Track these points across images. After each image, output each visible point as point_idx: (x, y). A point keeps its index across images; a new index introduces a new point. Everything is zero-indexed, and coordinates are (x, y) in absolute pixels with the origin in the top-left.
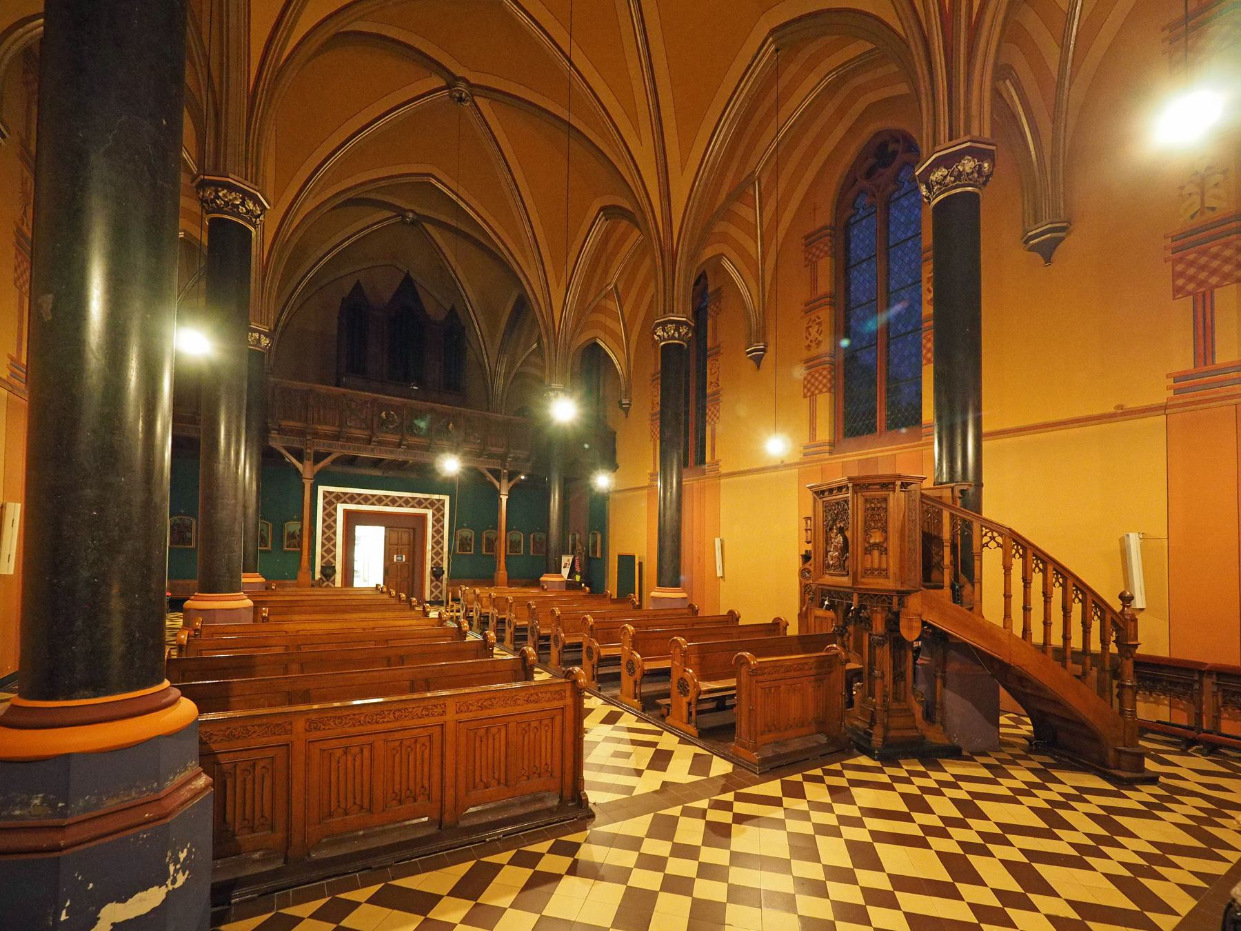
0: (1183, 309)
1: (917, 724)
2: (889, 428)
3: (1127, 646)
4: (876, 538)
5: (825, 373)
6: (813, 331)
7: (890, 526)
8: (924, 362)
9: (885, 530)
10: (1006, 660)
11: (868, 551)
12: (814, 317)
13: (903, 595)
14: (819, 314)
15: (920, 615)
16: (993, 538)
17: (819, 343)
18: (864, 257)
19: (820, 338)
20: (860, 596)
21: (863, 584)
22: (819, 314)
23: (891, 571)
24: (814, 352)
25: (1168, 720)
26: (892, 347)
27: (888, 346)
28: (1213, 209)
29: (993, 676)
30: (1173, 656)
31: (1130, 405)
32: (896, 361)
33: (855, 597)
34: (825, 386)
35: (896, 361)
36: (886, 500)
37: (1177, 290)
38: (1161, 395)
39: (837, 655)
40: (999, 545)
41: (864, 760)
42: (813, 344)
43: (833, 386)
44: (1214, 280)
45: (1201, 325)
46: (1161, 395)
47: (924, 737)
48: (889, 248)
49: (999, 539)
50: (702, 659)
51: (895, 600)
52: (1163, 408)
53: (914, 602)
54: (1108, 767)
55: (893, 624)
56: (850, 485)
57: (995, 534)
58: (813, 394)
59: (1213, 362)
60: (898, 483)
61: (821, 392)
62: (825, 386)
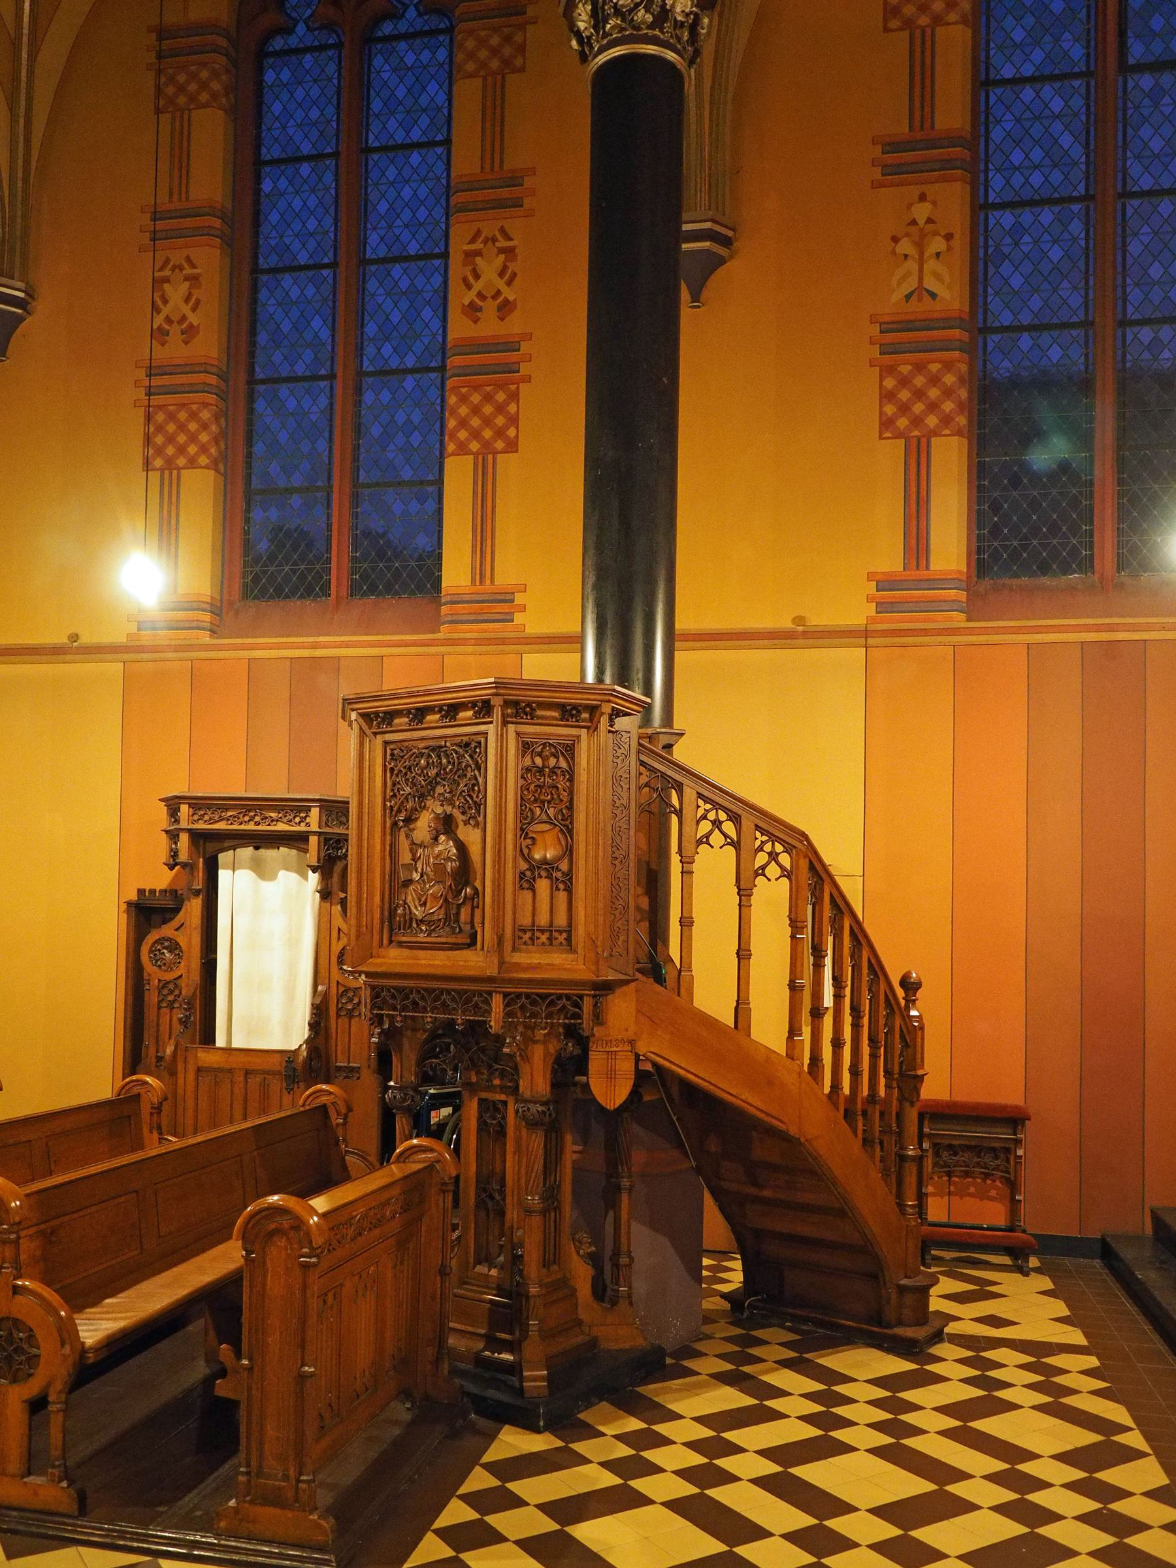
0: (890, 456)
1: (583, 1315)
2: (355, 590)
3: (908, 1078)
4: (546, 851)
5: (205, 415)
6: (176, 292)
7: (580, 817)
8: (451, 447)
9: (567, 828)
10: (793, 1131)
11: (526, 881)
12: (177, 257)
13: (604, 988)
14: (194, 253)
15: (632, 1042)
16: (773, 856)
17: (190, 332)
18: (306, 149)
19: (509, 294)
20: (510, 1000)
21: (517, 967)
22: (194, 253)
23: (580, 932)
24: (175, 351)
25: (945, 1220)
26: (368, 397)
27: (358, 391)
28: (933, 296)
29: (698, 1170)
30: (958, 1098)
31: (819, 619)
32: (376, 431)
33: (497, 1002)
34: (204, 449)
35: (376, 431)
36: (569, 750)
37: (886, 424)
38: (857, 611)
39: (430, 1168)
40: (786, 874)
41: (514, 1442)
42: (175, 330)
43: (223, 456)
44: (932, 421)
45: (914, 497)
46: (857, 611)
47: (593, 1343)
48: (259, 163)
49: (785, 859)
50: (48, 1237)
51: (587, 1004)
52: (862, 635)
53: (622, 1010)
54: (889, 1327)
55: (571, 1068)
56: (496, 702)
57: (779, 848)
58: (487, 445)
59: (927, 568)
60: (607, 708)
61: (192, 463)
62: (204, 449)
